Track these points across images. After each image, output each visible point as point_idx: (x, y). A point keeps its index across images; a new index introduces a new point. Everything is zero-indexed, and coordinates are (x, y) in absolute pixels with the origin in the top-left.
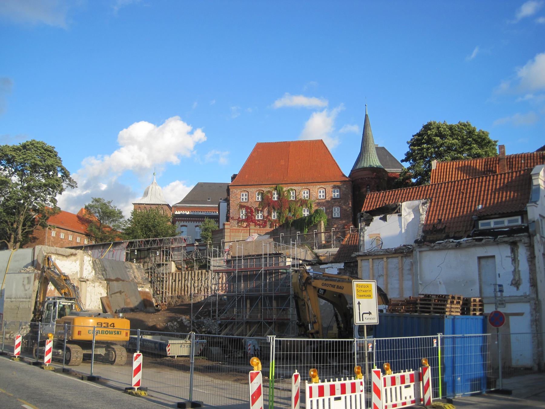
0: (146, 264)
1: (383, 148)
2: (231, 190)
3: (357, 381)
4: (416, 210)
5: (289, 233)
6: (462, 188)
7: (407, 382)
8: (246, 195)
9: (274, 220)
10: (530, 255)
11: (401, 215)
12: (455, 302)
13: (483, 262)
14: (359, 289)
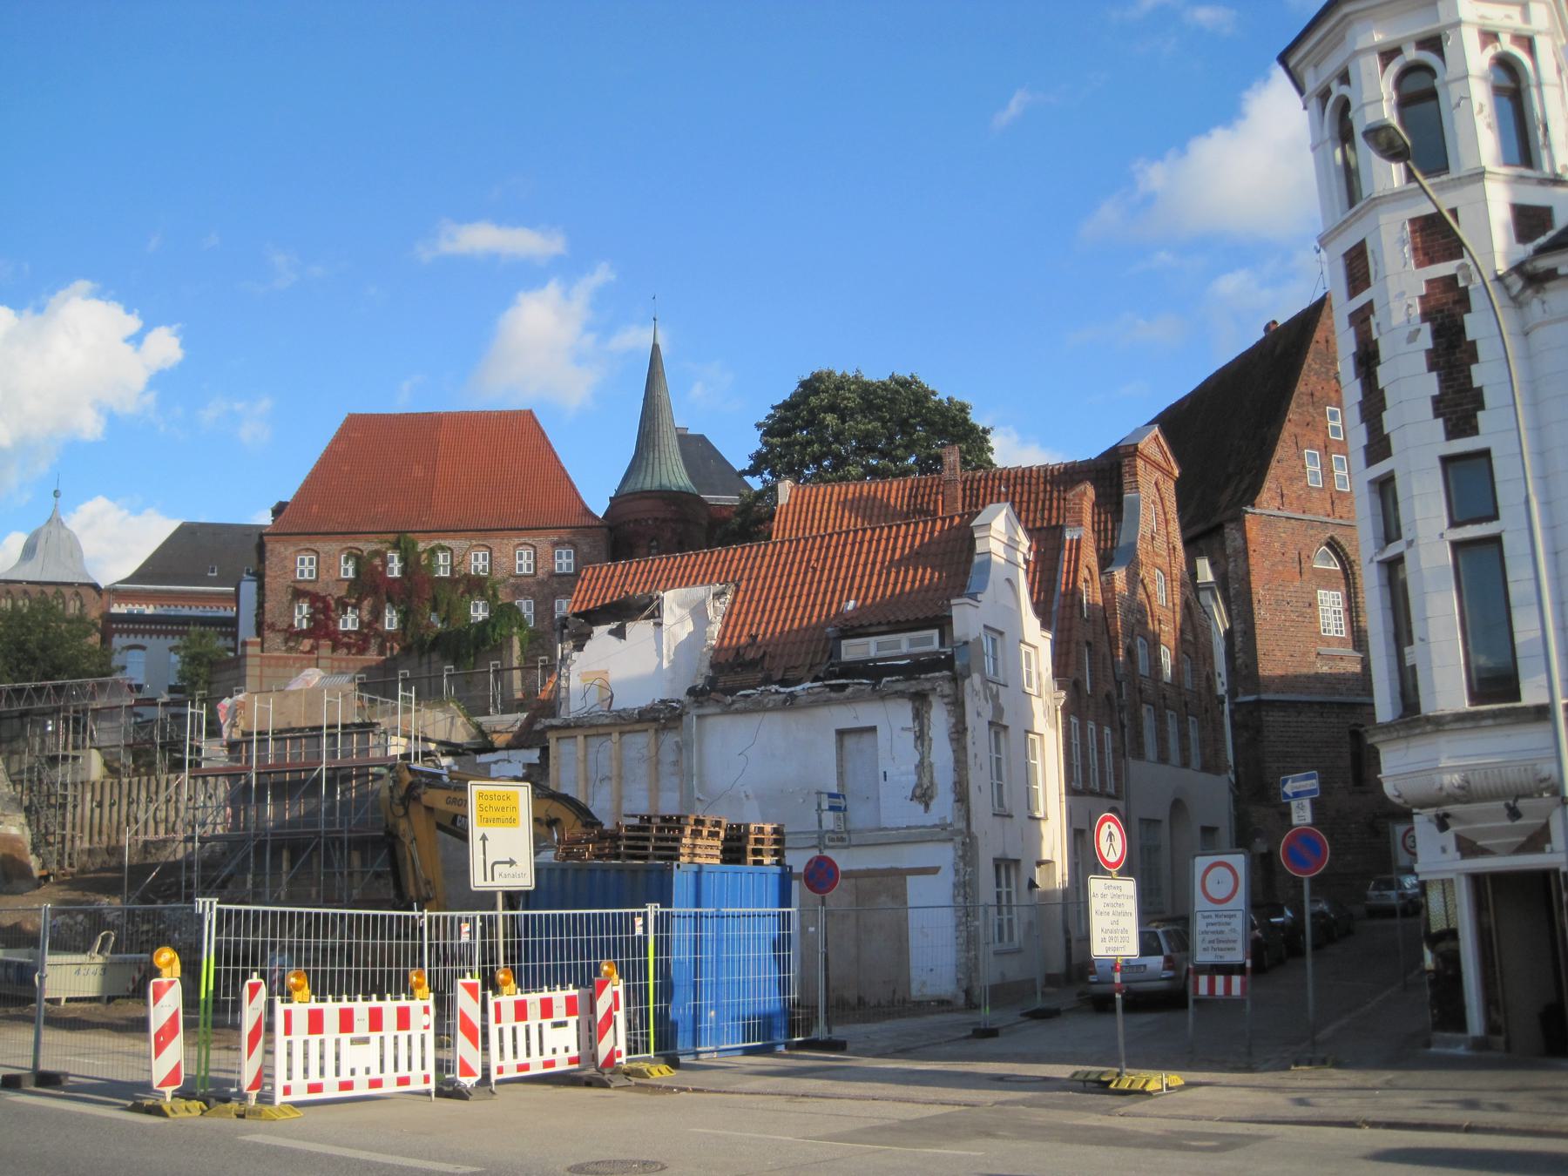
0: (16, 757)
1: (702, 438)
2: (269, 547)
3: (416, 1006)
4: (698, 613)
5: (425, 667)
6: (814, 556)
7: (559, 1013)
8: (311, 562)
9: (389, 632)
10: (955, 725)
11: (659, 625)
12: (705, 833)
13: (850, 742)
14: (486, 803)
